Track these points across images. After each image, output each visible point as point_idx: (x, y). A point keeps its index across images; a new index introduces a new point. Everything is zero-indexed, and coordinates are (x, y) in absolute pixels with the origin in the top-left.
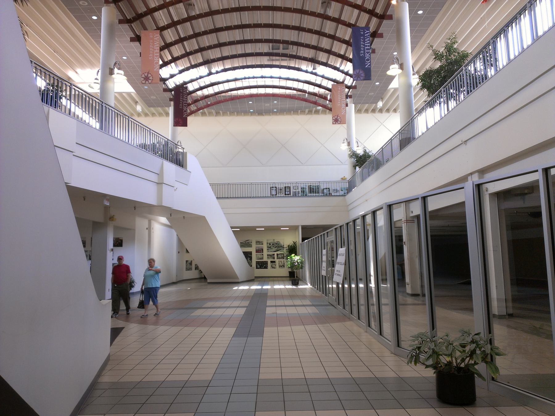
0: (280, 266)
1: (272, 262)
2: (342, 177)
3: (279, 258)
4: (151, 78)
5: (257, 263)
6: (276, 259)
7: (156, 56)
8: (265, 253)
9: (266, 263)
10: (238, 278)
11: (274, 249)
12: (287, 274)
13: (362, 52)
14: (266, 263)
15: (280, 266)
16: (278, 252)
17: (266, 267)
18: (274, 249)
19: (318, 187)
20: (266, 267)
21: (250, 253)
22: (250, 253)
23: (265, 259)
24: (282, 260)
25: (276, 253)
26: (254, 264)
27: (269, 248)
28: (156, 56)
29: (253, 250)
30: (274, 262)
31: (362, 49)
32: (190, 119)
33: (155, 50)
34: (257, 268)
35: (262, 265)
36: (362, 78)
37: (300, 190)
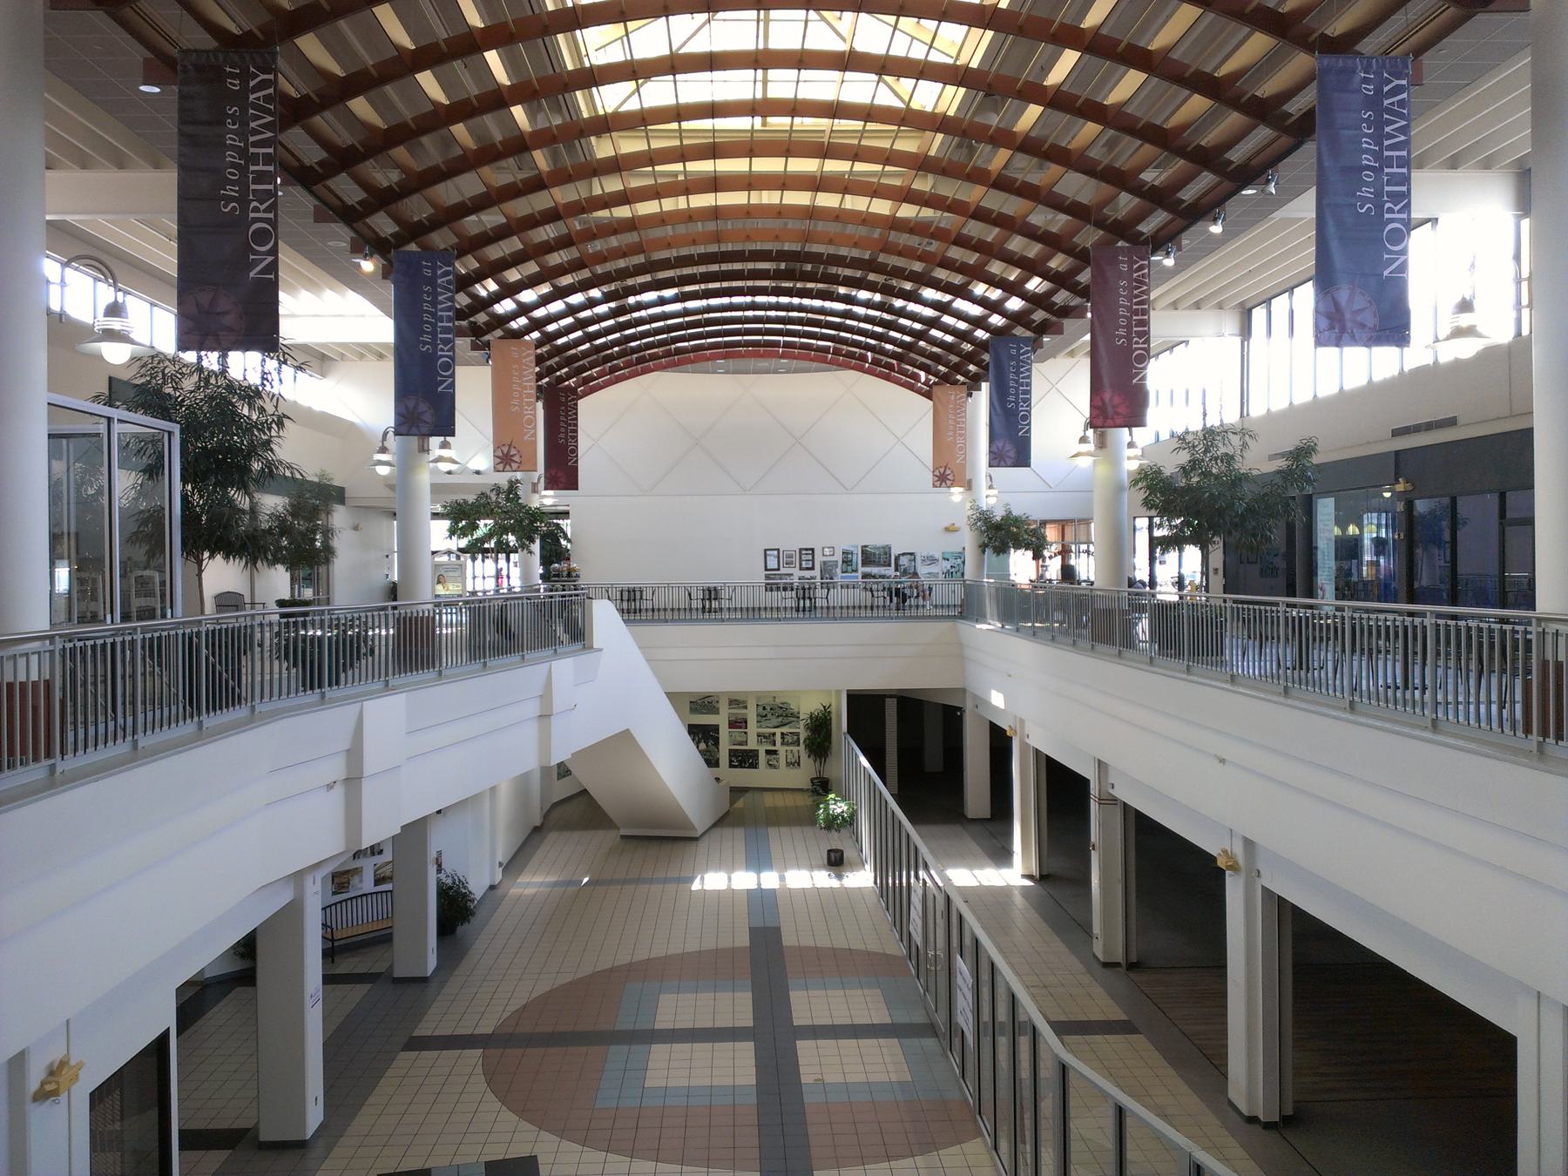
0: (789, 764)
1: (768, 752)
2: (947, 524)
3: (787, 744)
4: (516, 458)
5: (733, 753)
6: (778, 747)
7: (529, 396)
8: (753, 728)
9: (754, 754)
10: (693, 828)
11: (775, 721)
12: (806, 785)
13: (1012, 398)
14: (754, 754)
15: (789, 764)
16: (785, 730)
17: (754, 766)
18: (775, 721)
19: (887, 550)
20: (754, 766)
21: (716, 728)
22: (716, 728)
23: (752, 744)
24: (795, 749)
25: (778, 731)
26: (724, 756)
27: (762, 717)
28: (529, 396)
29: (721, 720)
30: (775, 752)
31: (1012, 391)
32: (743, 940)
33: (525, 388)
34: (731, 766)
35: (744, 759)
36: (1009, 462)
37: (839, 557)
